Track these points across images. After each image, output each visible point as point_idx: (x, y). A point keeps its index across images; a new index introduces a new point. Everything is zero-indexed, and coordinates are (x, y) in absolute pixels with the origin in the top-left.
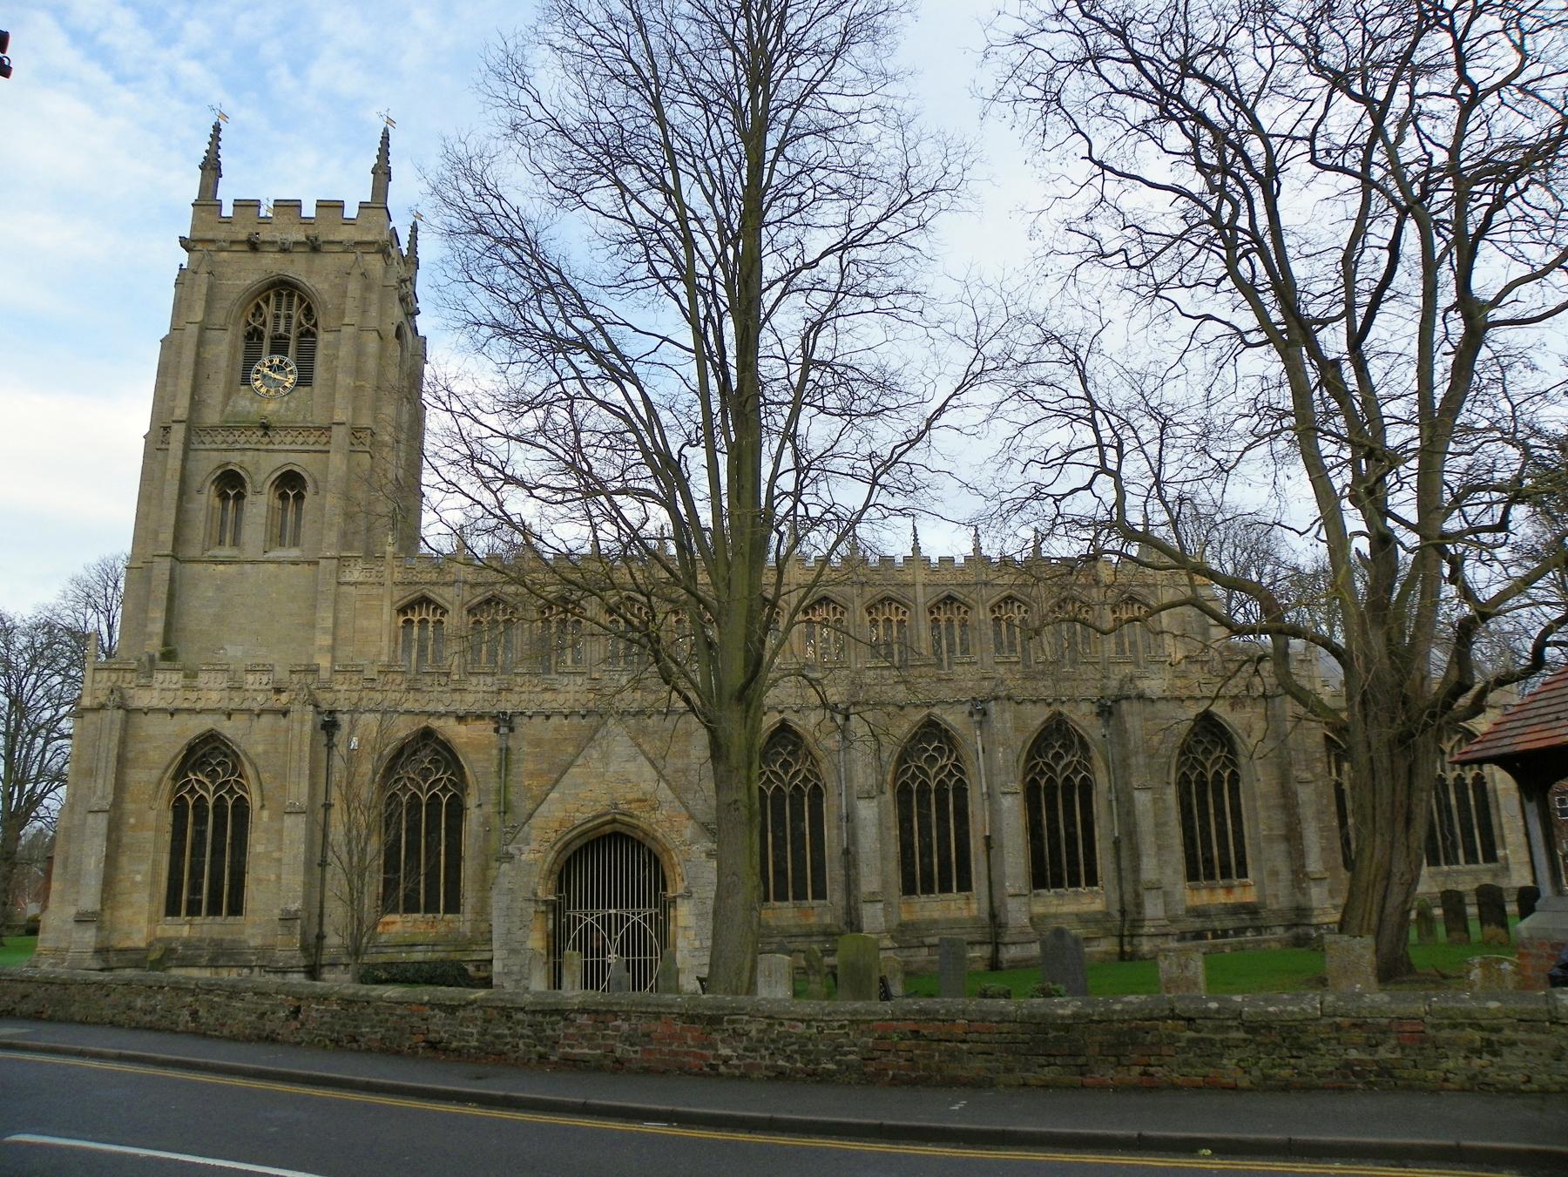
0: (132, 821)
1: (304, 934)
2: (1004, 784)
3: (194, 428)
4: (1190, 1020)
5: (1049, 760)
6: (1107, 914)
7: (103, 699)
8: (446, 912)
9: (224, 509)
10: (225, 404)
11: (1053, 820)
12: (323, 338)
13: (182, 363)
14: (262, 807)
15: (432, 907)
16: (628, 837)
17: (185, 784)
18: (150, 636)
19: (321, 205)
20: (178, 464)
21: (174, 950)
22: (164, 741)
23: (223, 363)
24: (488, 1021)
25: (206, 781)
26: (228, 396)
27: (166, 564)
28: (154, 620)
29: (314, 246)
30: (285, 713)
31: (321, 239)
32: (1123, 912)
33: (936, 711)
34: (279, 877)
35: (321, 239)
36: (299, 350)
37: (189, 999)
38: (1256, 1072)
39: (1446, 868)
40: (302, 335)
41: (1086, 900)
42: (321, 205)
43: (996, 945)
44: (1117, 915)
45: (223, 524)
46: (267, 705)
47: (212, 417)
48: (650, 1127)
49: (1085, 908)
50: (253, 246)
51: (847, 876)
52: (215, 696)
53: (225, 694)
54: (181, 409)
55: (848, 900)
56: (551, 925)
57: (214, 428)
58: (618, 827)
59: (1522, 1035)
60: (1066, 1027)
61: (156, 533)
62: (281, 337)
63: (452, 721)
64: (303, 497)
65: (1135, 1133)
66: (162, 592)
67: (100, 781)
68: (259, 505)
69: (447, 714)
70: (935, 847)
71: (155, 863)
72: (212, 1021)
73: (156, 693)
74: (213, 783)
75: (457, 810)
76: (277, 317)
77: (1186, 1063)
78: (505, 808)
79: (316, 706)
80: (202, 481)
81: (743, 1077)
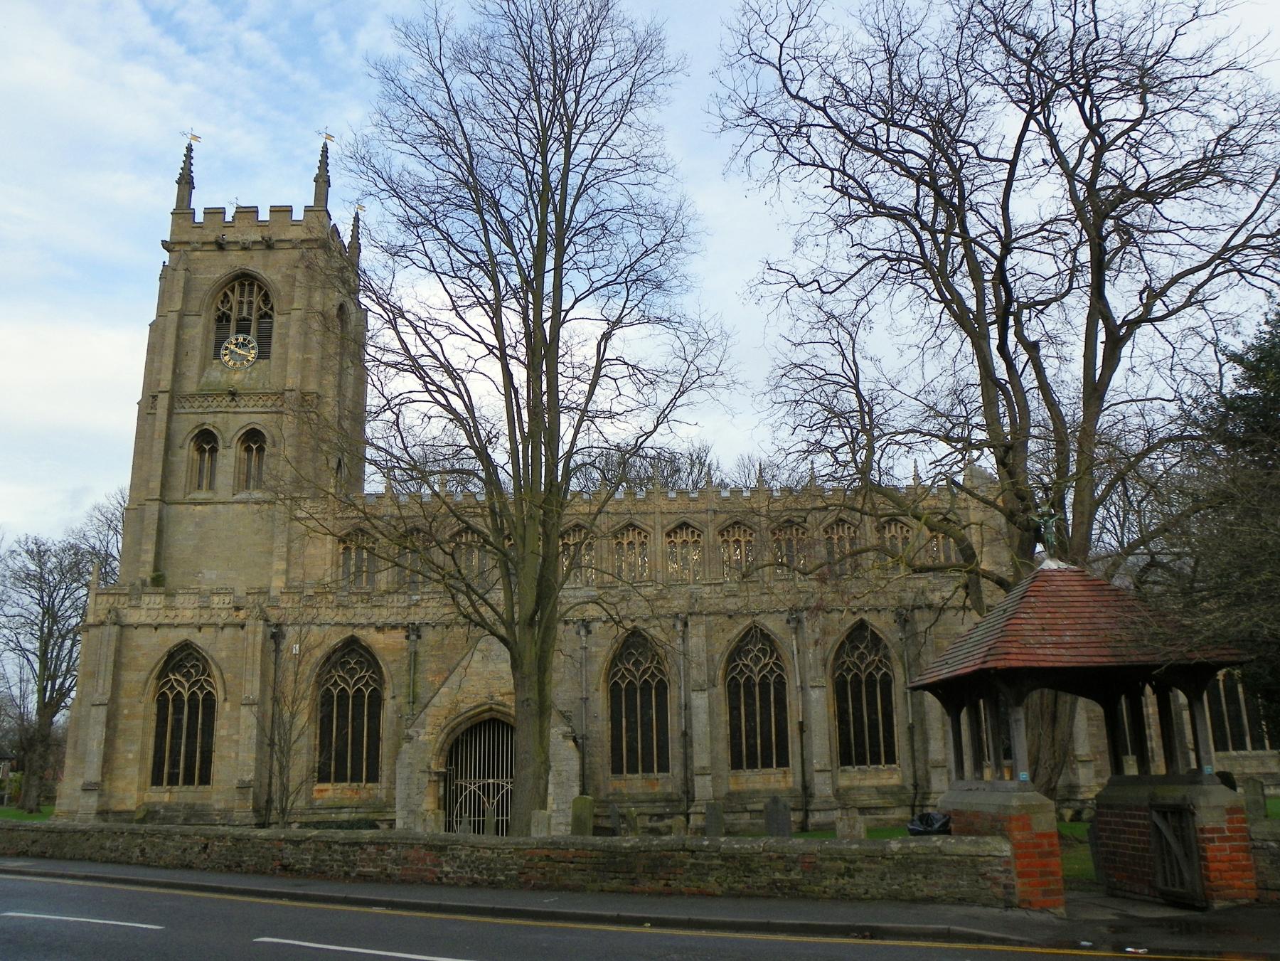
0: (126, 712)
1: (256, 799)
2: (813, 679)
3: (175, 396)
4: (693, 852)
5: (855, 659)
6: (902, 788)
7: (103, 618)
8: (368, 781)
9: (202, 460)
10: (201, 374)
11: (858, 709)
12: (278, 319)
13: (166, 343)
14: (225, 700)
15: (356, 778)
16: (503, 723)
17: (166, 683)
18: (144, 563)
19: (274, 210)
20: (164, 425)
21: (157, 812)
22: (150, 649)
23: (198, 343)
24: (317, 851)
25: (183, 680)
26: (203, 369)
27: (155, 507)
28: (147, 552)
29: (268, 245)
30: (243, 627)
31: (274, 239)
32: (916, 786)
33: (757, 618)
34: (237, 754)
35: (274, 239)
36: (259, 330)
37: (140, 841)
38: (725, 885)
39: (1234, 753)
40: (261, 317)
41: (886, 776)
42: (274, 210)
43: (807, 813)
44: (910, 788)
45: (201, 471)
46: (229, 620)
47: (190, 387)
48: (376, 910)
49: (884, 782)
50: (221, 246)
51: (685, 754)
52: (189, 613)
53: (197, 611)
54: (166, 382)
55: (686, 773)
56: (442, 791)
57: (193, 396)
58: (494, 714)
59: (865, 865)
60: (626, 854)
61: (148, 481)
62: (244, 319)
63: (372, 630)
64: (263, 450)
65: (615, 914)
66: (152, 530)
67: (101, 681)
68: (229, 457)
69: (370, 625)
70: (759, 729)
71: (144, 745)
72: (153, 856)
73: (143, 612)
74: (188, 681)
75: (377, 701)
76: (241, 303)
77: (689, 879)
78: (414, 700)
79: (266, 620)
80: (182, 437)
81: (456, 885)
